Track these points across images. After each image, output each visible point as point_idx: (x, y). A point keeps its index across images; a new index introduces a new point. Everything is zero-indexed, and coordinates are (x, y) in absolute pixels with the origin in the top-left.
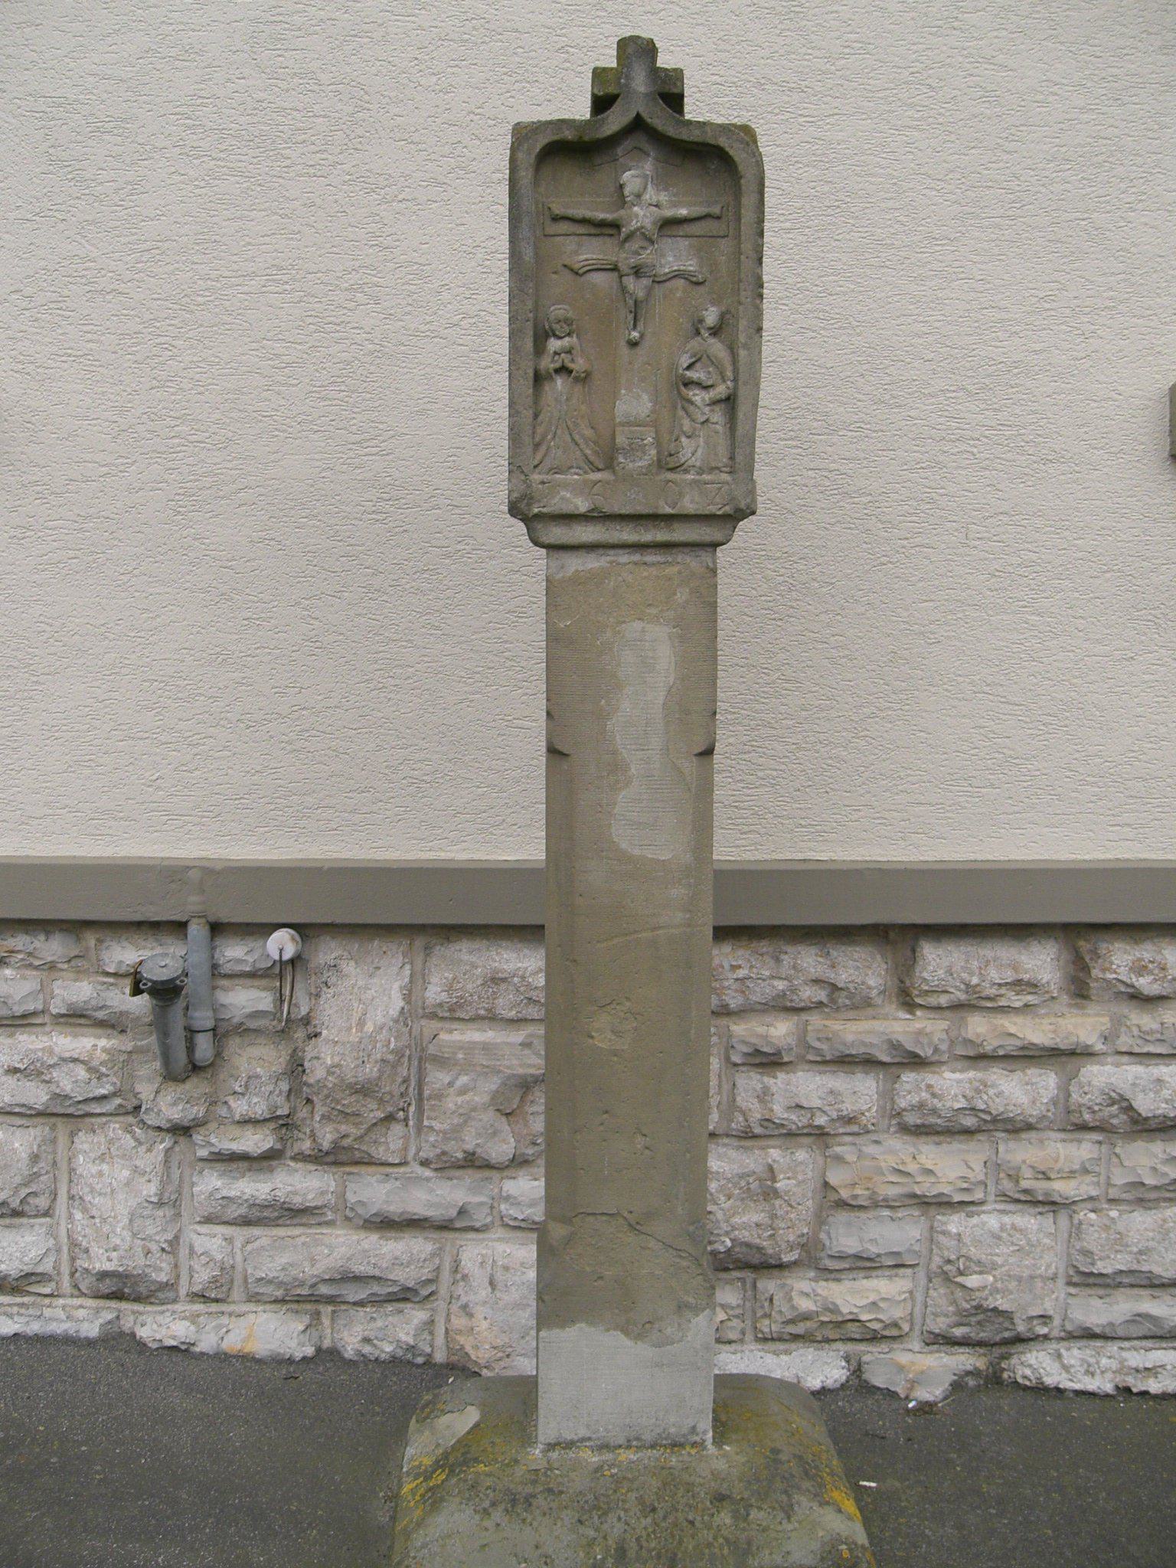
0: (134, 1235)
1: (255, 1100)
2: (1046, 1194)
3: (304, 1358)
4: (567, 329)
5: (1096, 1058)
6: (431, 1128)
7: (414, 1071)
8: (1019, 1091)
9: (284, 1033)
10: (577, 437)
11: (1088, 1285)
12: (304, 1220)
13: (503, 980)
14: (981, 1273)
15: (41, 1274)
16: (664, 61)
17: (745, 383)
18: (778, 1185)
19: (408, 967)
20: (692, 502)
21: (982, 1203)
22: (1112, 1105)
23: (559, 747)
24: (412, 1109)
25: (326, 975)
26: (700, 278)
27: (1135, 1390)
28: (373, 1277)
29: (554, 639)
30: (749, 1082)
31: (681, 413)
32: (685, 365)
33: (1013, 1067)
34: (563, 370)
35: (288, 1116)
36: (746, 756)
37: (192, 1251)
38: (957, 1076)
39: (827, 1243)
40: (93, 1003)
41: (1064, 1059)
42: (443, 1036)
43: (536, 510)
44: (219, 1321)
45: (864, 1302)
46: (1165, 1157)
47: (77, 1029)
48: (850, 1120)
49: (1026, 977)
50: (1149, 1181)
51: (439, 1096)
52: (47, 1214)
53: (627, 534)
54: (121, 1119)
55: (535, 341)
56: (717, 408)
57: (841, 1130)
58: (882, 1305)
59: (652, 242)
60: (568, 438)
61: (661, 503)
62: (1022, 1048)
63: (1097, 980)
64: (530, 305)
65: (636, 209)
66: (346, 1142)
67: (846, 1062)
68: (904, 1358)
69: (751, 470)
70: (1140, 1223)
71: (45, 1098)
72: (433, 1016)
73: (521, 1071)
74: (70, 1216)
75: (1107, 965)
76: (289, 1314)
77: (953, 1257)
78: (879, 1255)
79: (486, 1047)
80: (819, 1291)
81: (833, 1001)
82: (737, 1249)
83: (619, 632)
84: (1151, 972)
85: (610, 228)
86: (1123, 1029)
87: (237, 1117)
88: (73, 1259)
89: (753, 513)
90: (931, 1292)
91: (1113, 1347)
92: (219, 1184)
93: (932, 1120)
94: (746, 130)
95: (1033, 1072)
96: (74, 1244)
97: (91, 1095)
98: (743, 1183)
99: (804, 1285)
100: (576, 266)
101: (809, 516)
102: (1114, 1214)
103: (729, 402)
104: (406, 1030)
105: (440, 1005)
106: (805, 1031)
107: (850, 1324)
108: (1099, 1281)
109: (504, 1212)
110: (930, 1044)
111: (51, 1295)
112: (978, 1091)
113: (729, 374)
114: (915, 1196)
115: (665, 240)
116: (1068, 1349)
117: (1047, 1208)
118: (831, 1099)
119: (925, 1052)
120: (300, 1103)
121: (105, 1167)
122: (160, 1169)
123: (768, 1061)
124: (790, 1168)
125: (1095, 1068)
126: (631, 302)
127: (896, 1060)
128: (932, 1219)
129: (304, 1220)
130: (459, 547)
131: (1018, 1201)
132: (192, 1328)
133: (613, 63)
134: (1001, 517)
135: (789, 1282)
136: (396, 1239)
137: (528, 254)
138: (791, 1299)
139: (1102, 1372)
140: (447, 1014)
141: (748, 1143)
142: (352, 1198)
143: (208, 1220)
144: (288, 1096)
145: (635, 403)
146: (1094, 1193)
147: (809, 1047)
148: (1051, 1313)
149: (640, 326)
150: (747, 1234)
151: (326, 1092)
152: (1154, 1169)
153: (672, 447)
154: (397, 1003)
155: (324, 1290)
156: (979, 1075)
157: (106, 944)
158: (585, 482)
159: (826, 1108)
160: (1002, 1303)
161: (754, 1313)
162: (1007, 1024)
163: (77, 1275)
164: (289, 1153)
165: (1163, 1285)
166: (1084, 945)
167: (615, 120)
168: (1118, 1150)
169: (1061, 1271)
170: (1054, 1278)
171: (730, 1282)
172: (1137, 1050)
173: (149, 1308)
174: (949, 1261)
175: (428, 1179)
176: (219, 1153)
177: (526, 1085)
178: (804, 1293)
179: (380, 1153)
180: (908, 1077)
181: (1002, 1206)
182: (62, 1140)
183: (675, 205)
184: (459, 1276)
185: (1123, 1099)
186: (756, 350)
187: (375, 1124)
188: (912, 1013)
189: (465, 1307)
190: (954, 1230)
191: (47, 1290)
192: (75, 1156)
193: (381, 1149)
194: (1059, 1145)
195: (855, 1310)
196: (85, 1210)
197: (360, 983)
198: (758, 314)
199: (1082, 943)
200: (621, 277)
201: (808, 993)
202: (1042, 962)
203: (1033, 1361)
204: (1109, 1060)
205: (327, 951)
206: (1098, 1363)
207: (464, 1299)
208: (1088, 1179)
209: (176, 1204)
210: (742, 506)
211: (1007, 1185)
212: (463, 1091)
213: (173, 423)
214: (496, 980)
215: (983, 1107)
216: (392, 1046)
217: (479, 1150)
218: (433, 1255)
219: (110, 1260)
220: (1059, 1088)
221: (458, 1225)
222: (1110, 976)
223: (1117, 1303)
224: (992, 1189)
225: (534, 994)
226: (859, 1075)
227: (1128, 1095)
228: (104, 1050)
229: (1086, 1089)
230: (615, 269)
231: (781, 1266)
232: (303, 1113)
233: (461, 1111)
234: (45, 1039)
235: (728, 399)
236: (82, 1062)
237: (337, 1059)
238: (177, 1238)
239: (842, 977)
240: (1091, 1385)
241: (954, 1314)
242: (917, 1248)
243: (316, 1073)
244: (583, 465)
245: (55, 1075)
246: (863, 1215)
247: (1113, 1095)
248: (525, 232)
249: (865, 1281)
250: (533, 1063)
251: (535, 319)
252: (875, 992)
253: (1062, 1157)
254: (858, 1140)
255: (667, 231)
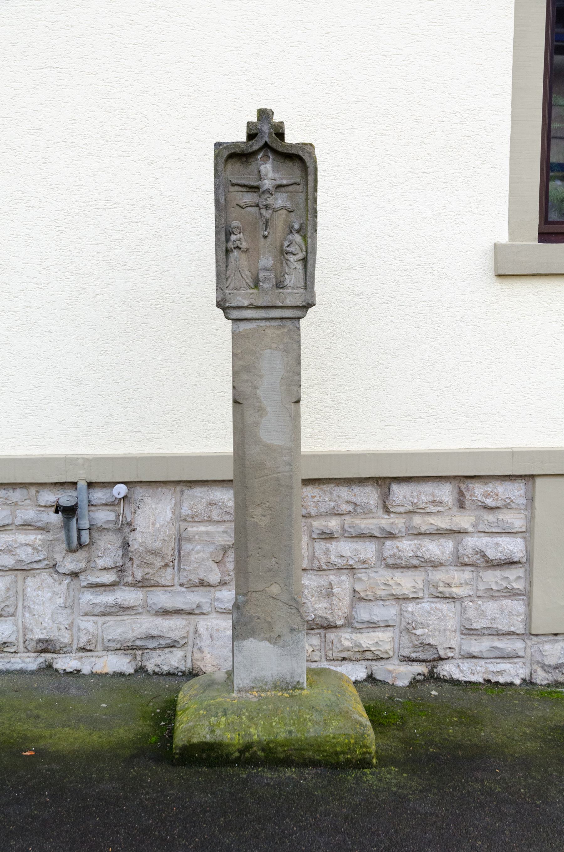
0: (53, 622)
1: (108, 559)
2: (450, 594)
3: (129, 675)
4: (239, 231)
5: (468, 534)
6: (184, 569)
7: (176, 544)
8: (435, 549)
9: (120, 530)
10: (243, 275)
11: (470, 635)
12: (129, 613)
13: (215, 504)
14: (423, 628)
15: (10, 643)
16: (276, 119)
18: (334, 590)
19: (173, 499)
21: (422, 598)
22: (477, 554)
23: (238, 401)
24: (176, 561)
25: (138, 503)
27: (493, 681)
28: (160, 636)
29: (235, 357)
30: (320, 546)
31: (285, 265)
32: (286, 245)
33: (433, 539)
34: (238, 248)
35: (122, 566)
36: (316, 407)
37: (79, 629)
38: (409, 542)
39: (356, 616)
40: (35, 519)
41: (456, 535)
42: (189, 529)
43: (227, 305)
44: (91, 660)
45: (373, 642)
46: (501, 577)
47: (28, 531)
48: (364, 562)
49: (437, 499)
50: (494, 588)
51: (188, 555)
52: (13, 615)
54: (47, 570)
55: (226, 235)
56: (299, 263)
57: (360, 567)
58: (380, 643)
61: (278, 301)
62: (437, 530)
63: (468, 500)
64: (223, 221)
66: (147, 577)
67: (361, 536)
68: (391, 667)
70: (491, 607)
71: (13, 562)
72: (185, 520)
73: (223, 543)
74: (24, 616)
75: (473, 494)
76: (122, 655)
77: (410, 622)
78: (378, 622)
79: (208, 533)
80: (353, 638)
81: (355, 510)
82: (317, 619)
84: (492, 497)
85: (254, 189)
86: (481, 522)
87: (100, 567)
88: (25, 635)
89: (315, 305)
90: (402, 638)
91: (482, 662)
92: (91, 597)
93: (399, 561)
94: (311, 145)
95: (442, 540)
96: (25, 628)
97: (34, 560)
98: (319, 590)
99: (347, 635)
100: (242, 205)
102: (480, 603)
103: (305, 260)
104: (173, 527)
105: (188, 515)
106: (344, 524)
107: (367, 652)
108: (475, 632)
109: (217, 606)
110: (397, 528)
111: (15, 652)
112: (418, 549)
113: (304, 249)
114: (393, 595)
116: (463, 663)
117: (451, 600)
118: (355, 552)
119: (395, 532)
120: (127, 560)
121: (40, 592)
122: (65, 592)
123: (328, 536)
124: (338, 583)
125: (469, 539)
126: (264, 220)
127: (384, 536)
128: (401, 606)
129: (129, 613)
130: (193, 319)
131: (438, 597)
132: (79, 663)
134: (423, 303)
135: (340, 634)
136: (169, 619)
137: (222, 201)
138: (341, 641)
139: (478, 673)
140: (191, 520)
141: (321, 573)
142: (150, 602)
143: (86, 614)
144: (122, 557)
146: (471, 594)
147: (345, 531)
148: (454, 646)
149: (268, 229)
150: (321, 612)
151: (139, 554)
152: (497, 583)
153: (282, 279)
154: (169, 515)
155: (138, 643)
156: (419, 542)
157: (40, 493)
158: (247, 293)
159: (354, 557)
160: (432, 642)
161: (325, 648)
162: (430, 519)
163: (27, 642)
164: (122, 583)
165: (503, 634)
166: (463, 486)
167: (257, 145)
168: (480, 574)
169: (458, 628)
170: (455, 631)
171: (315, 634)
172: (487, 531)
173: (59, 656)
174: (409, 623)
175: (183, 592)
176: (91, 584)
177: (225, 550)
178: (346, 639)
179: (162, 581)
180: (389, 543)
181: (431, 600)
182: (20, 582)
184: (197, 635)
185: (481, 551)
186: (314, 239)
187: (160, 568)
188: (389, 515)
189: (200, 649)
190: (411, 610)
191: (13, 650)
192: (26, 588)
193: (163, 579)
194: (455, 572)
195: (369, 646)
196: (30, 612)
197: (153, 507)
199: (462, 485)
200: (260, 209)
201: (344, 507)
202: (446, 493)
203: (447, 668)
204: (475, 535)
205: (139, 492)
206: (476, 669)
207: (199, 645)
208: (468, 587)
209: (72, 607)
211: (432, 590)
212: (198, 553)
213: (66, 266)
214: (211, 504)
215: (421, 555)
216: (167, 533)
217: (205, 578)
218: (186, 626)
219: (42, 634)
220: (454, 548)
221: (196, 612)
222: (474, 498)
223: (483, 642)
224: (426, 592)
225: (228, 510)
226: (367, 543)
227: (484, 550)
228: (40, 540)
229: (465, 547)
230: (258, 206)
231: (336, 627)
232: (129, 564)
233: (197, 561)
234: (13, 536)
235: (304, 259)
236: (30, 545)
237: (143, 540)
238: (72, 623)
239: (359, 500)
240: (473, 679)
241: (412, 647)
242: (395, 618)
243: (134, 546)
244: (246, 286)
245: (18, 551)
246: (371, 604)
247: (477, 550)
249: (372, 633)
250: (229, 539)
251: (226, 227)
252: (373, 507)
253: (456, 577)
254: (367, 571)
255: (278, 190)
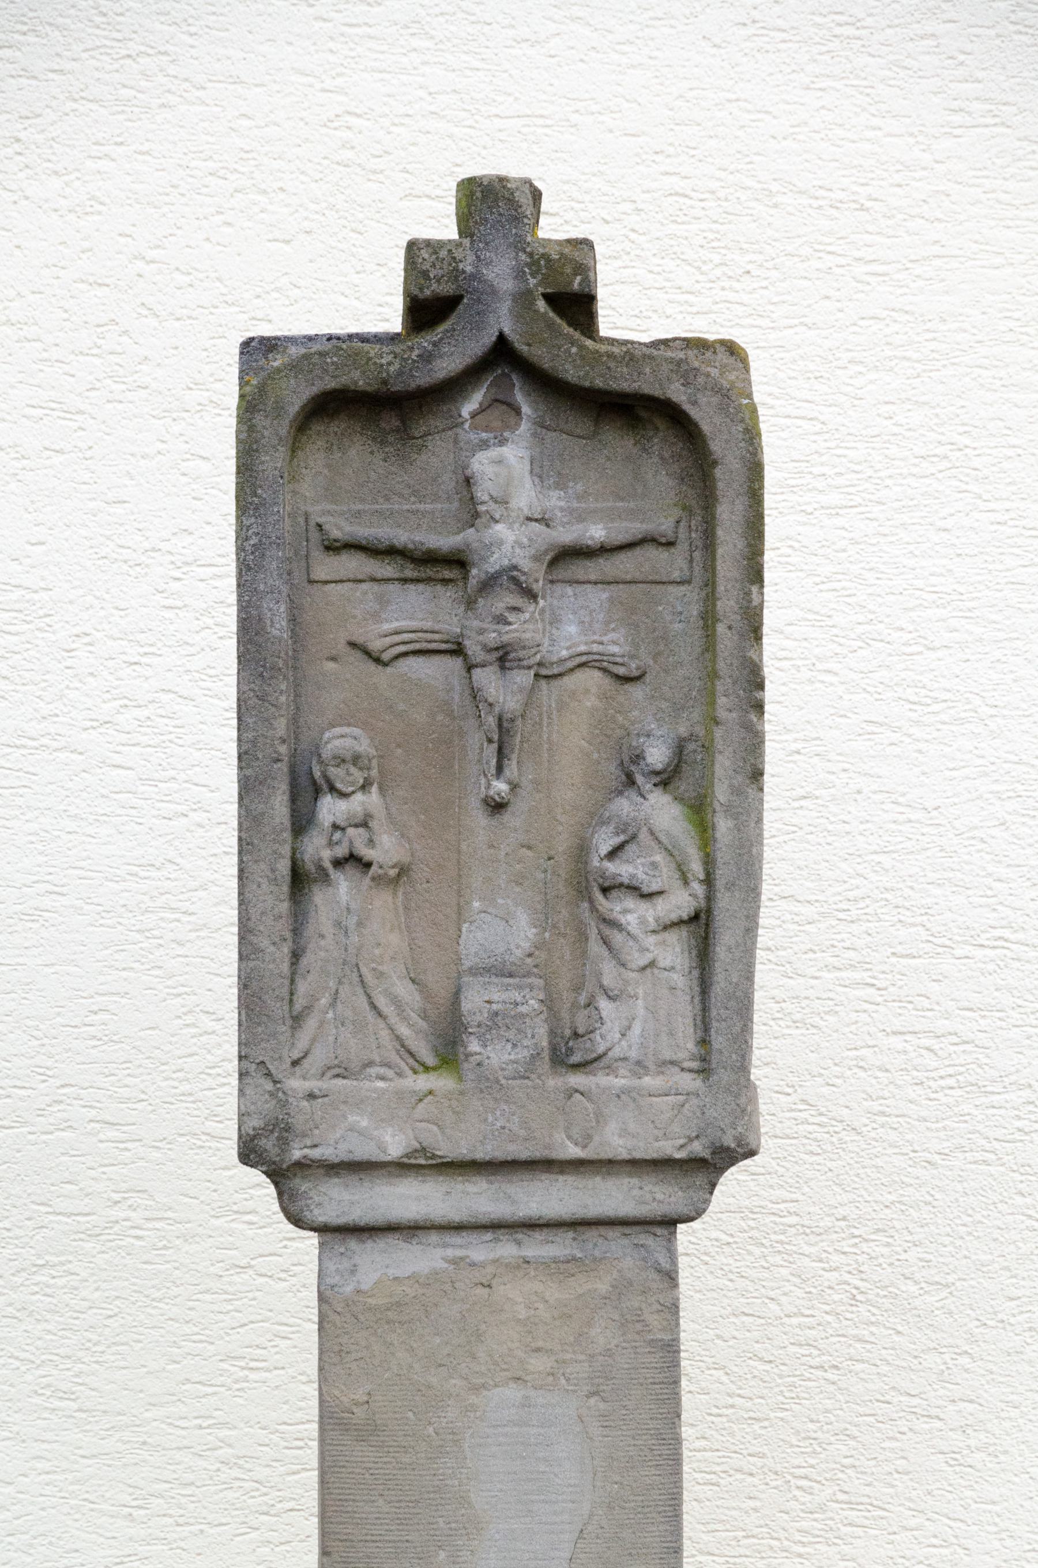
4: (359, 777)
10: (381, 1002)
16: (553, 227)
17: (730, 886)
20: (624, 1133)
26: (633, 668)
29: (333, 1421)
31: (595, 947)
34: (353, 861)
53: (479, 1197)
55: (294, 799)
56: (672, 937)
59: (531, 595)
60: (362, 1002)
61: (560, 1137)
64: (281, 726)
65: (499, 527)
69: (743, 1067)
83: (473, 1408)
89: (752, 1153)
94: (731, 348)
100: (376, 645)
101: (893, 1136)
103: (700, 924)
113: (696, 868)
115: (559, 588)
126: (491, 721)
133: (447, 230)
137: (278, 626)
145: (504, 926)
149: (512, 769)
158: (400, 1095)
167: (454, 351)
183: (581, 517)
198: (753, 745)
200: (470, 668)
210: (729, 1142)
230: (457, 650)
235: (695, 918)
248: (272, 578)
255: (563, 572)
